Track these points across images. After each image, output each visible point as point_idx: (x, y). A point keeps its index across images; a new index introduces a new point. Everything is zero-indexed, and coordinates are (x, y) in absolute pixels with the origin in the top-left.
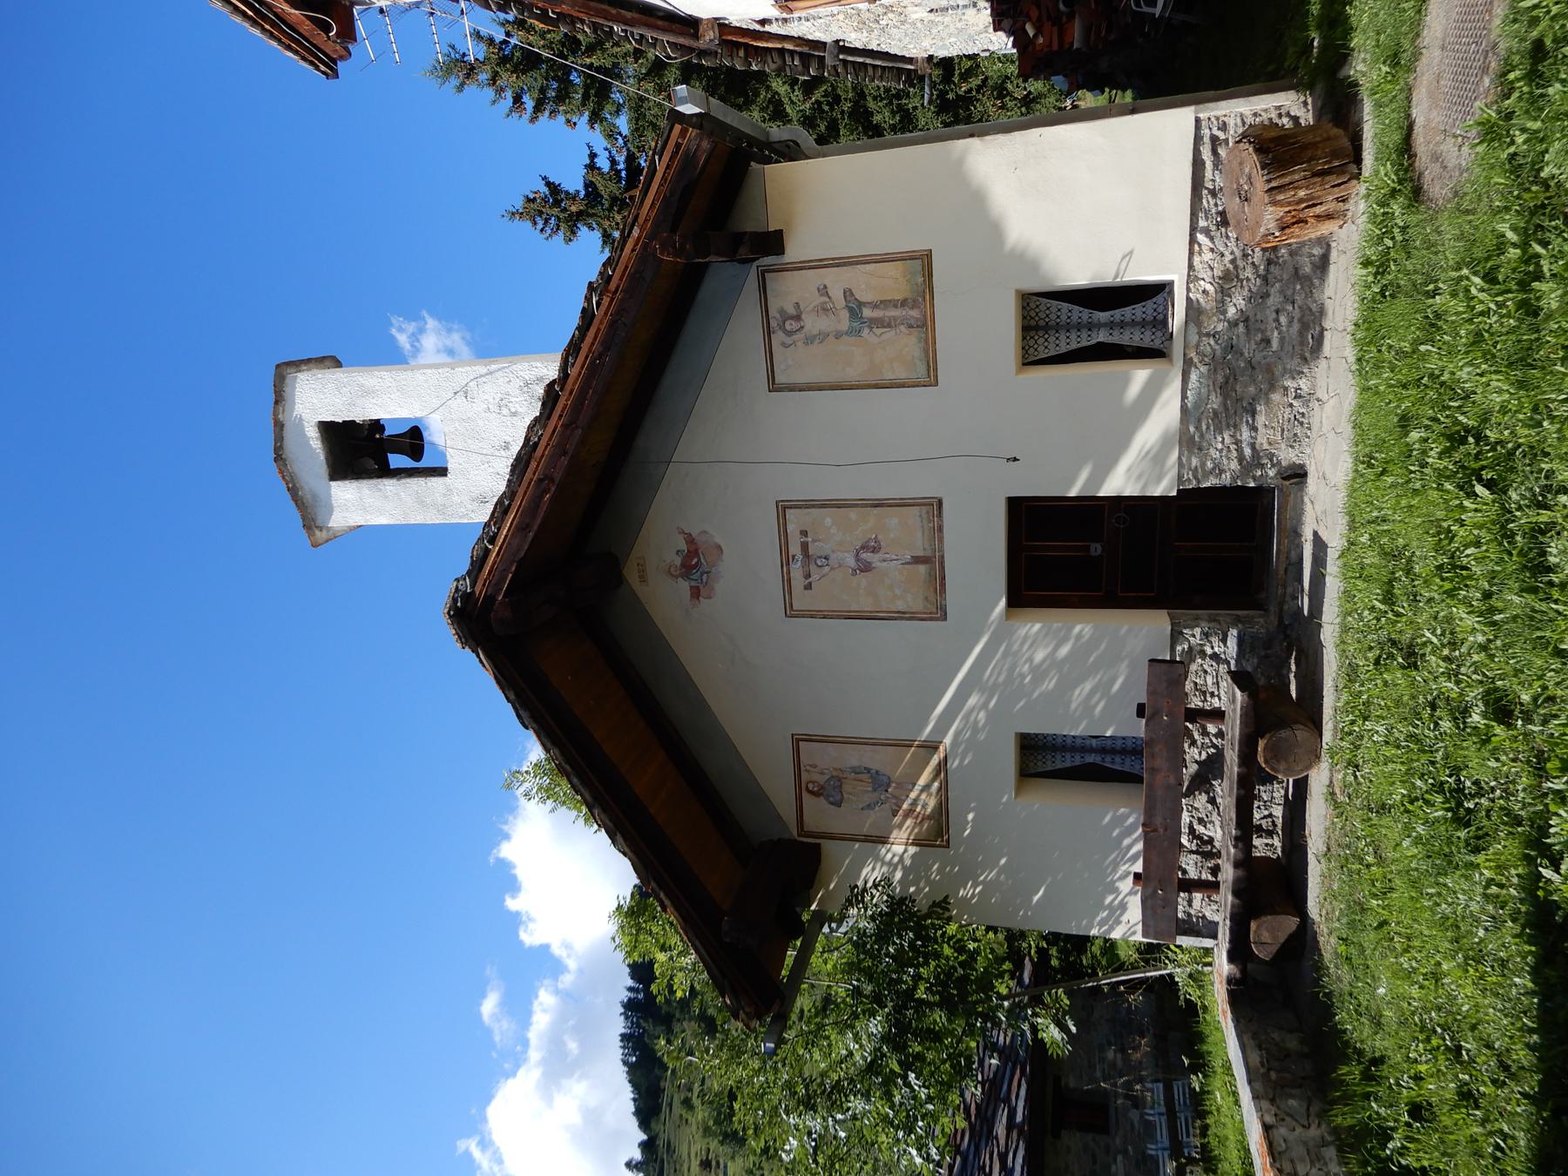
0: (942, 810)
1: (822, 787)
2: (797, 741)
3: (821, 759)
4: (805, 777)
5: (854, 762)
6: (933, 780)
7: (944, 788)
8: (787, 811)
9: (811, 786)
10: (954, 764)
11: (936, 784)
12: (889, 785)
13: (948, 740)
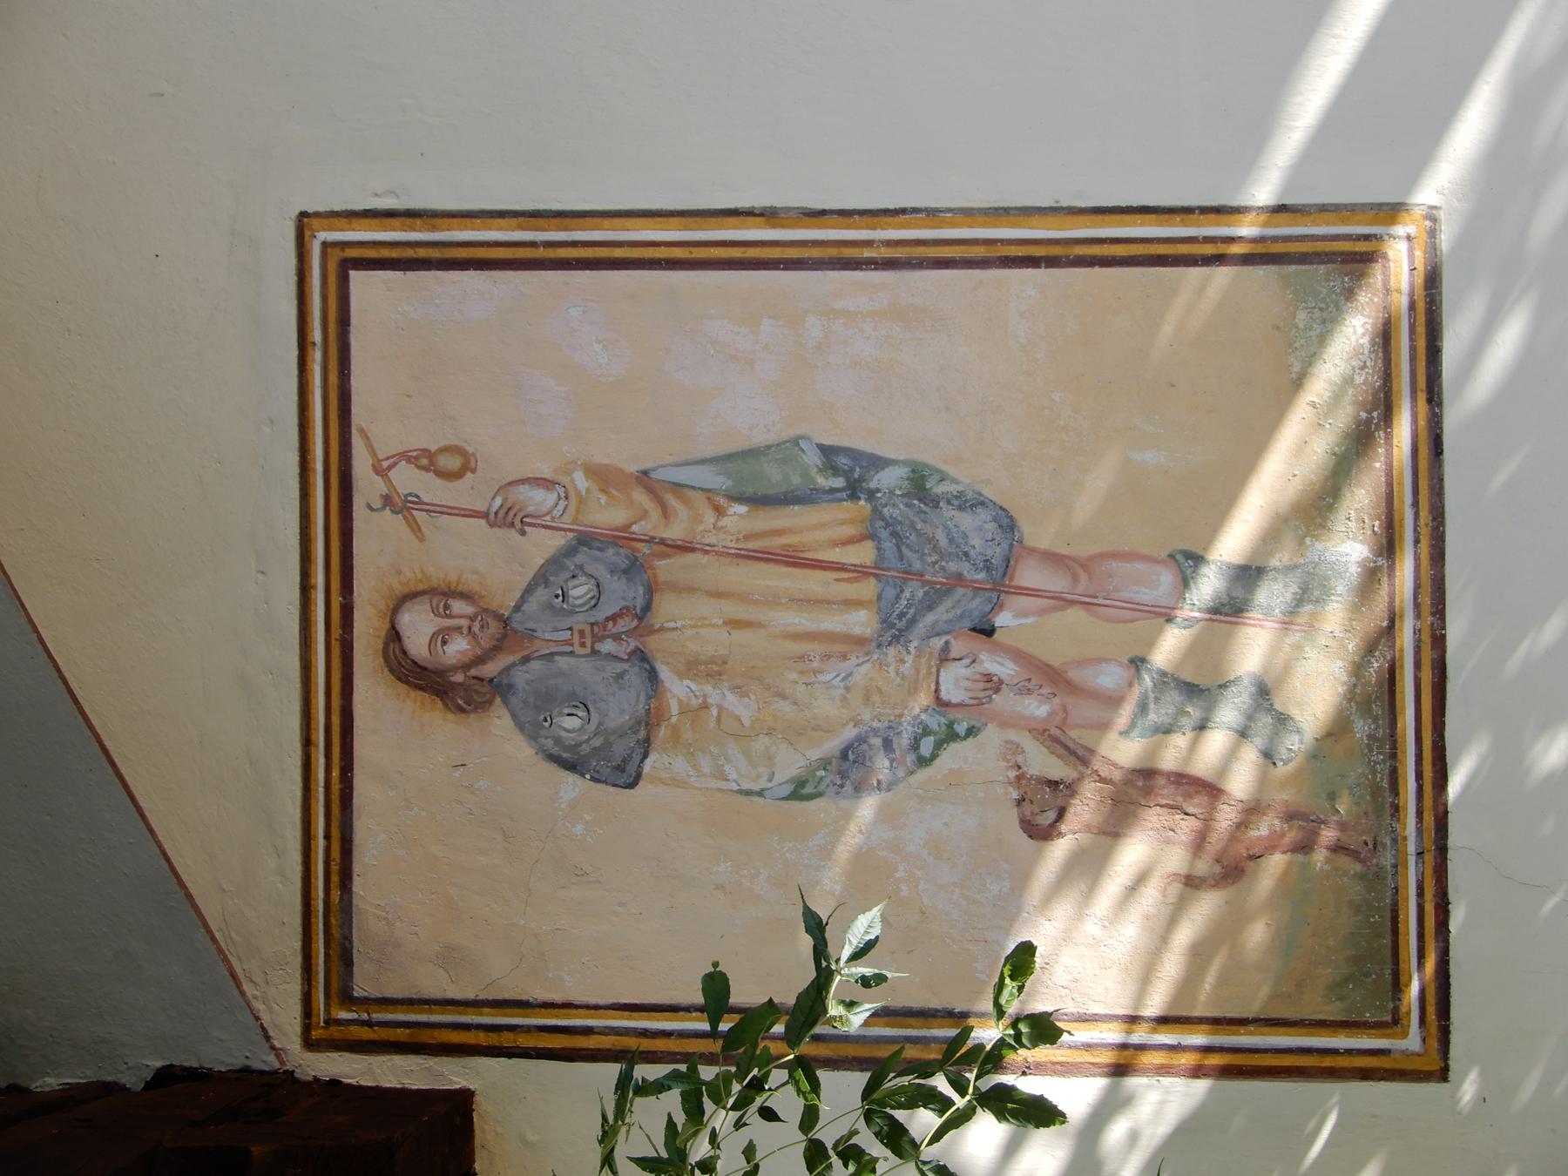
0: (1404, 704)
1: (506, 632)
2: (338, 261)
3: (510, 396)
4: (380, 547)
5: (748, 413)
6: (1362, 439)
7: (1420, 521)
8: (239, 861)
9: (418, 628)
10: (1489, 355)
11: (1361, 498)
12: (1000, 582)
13: (1439, 187)
